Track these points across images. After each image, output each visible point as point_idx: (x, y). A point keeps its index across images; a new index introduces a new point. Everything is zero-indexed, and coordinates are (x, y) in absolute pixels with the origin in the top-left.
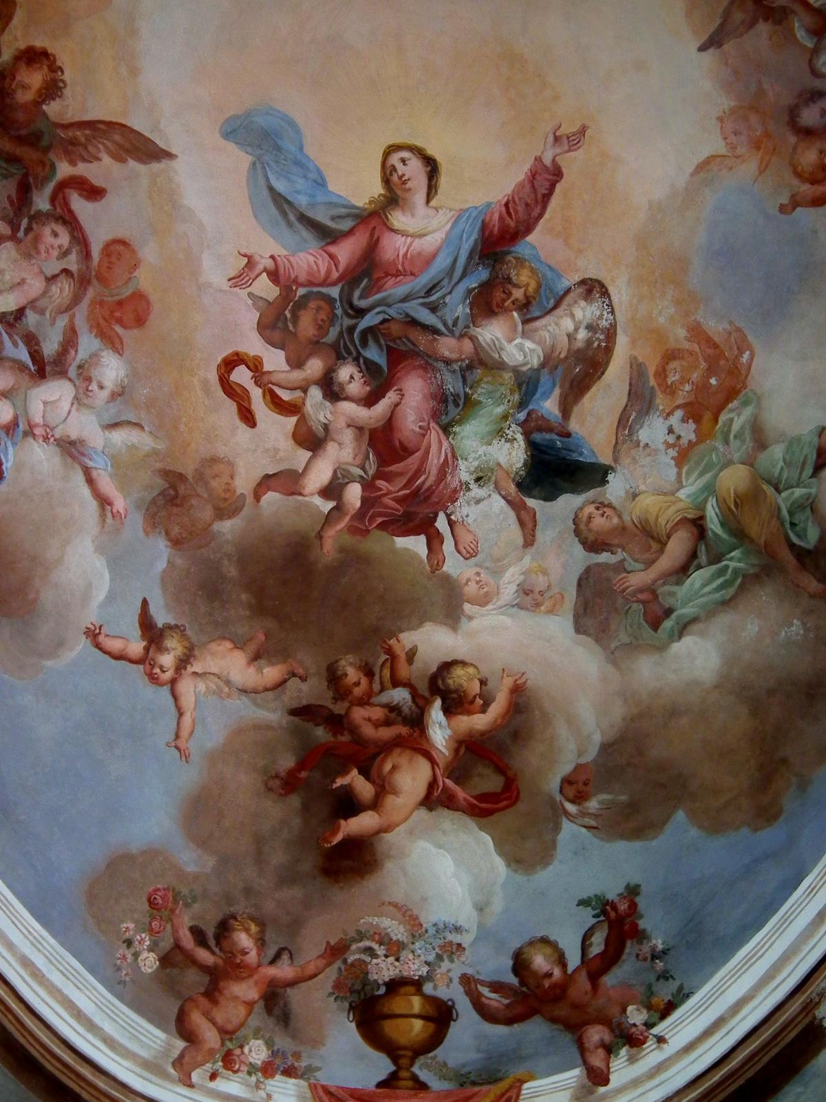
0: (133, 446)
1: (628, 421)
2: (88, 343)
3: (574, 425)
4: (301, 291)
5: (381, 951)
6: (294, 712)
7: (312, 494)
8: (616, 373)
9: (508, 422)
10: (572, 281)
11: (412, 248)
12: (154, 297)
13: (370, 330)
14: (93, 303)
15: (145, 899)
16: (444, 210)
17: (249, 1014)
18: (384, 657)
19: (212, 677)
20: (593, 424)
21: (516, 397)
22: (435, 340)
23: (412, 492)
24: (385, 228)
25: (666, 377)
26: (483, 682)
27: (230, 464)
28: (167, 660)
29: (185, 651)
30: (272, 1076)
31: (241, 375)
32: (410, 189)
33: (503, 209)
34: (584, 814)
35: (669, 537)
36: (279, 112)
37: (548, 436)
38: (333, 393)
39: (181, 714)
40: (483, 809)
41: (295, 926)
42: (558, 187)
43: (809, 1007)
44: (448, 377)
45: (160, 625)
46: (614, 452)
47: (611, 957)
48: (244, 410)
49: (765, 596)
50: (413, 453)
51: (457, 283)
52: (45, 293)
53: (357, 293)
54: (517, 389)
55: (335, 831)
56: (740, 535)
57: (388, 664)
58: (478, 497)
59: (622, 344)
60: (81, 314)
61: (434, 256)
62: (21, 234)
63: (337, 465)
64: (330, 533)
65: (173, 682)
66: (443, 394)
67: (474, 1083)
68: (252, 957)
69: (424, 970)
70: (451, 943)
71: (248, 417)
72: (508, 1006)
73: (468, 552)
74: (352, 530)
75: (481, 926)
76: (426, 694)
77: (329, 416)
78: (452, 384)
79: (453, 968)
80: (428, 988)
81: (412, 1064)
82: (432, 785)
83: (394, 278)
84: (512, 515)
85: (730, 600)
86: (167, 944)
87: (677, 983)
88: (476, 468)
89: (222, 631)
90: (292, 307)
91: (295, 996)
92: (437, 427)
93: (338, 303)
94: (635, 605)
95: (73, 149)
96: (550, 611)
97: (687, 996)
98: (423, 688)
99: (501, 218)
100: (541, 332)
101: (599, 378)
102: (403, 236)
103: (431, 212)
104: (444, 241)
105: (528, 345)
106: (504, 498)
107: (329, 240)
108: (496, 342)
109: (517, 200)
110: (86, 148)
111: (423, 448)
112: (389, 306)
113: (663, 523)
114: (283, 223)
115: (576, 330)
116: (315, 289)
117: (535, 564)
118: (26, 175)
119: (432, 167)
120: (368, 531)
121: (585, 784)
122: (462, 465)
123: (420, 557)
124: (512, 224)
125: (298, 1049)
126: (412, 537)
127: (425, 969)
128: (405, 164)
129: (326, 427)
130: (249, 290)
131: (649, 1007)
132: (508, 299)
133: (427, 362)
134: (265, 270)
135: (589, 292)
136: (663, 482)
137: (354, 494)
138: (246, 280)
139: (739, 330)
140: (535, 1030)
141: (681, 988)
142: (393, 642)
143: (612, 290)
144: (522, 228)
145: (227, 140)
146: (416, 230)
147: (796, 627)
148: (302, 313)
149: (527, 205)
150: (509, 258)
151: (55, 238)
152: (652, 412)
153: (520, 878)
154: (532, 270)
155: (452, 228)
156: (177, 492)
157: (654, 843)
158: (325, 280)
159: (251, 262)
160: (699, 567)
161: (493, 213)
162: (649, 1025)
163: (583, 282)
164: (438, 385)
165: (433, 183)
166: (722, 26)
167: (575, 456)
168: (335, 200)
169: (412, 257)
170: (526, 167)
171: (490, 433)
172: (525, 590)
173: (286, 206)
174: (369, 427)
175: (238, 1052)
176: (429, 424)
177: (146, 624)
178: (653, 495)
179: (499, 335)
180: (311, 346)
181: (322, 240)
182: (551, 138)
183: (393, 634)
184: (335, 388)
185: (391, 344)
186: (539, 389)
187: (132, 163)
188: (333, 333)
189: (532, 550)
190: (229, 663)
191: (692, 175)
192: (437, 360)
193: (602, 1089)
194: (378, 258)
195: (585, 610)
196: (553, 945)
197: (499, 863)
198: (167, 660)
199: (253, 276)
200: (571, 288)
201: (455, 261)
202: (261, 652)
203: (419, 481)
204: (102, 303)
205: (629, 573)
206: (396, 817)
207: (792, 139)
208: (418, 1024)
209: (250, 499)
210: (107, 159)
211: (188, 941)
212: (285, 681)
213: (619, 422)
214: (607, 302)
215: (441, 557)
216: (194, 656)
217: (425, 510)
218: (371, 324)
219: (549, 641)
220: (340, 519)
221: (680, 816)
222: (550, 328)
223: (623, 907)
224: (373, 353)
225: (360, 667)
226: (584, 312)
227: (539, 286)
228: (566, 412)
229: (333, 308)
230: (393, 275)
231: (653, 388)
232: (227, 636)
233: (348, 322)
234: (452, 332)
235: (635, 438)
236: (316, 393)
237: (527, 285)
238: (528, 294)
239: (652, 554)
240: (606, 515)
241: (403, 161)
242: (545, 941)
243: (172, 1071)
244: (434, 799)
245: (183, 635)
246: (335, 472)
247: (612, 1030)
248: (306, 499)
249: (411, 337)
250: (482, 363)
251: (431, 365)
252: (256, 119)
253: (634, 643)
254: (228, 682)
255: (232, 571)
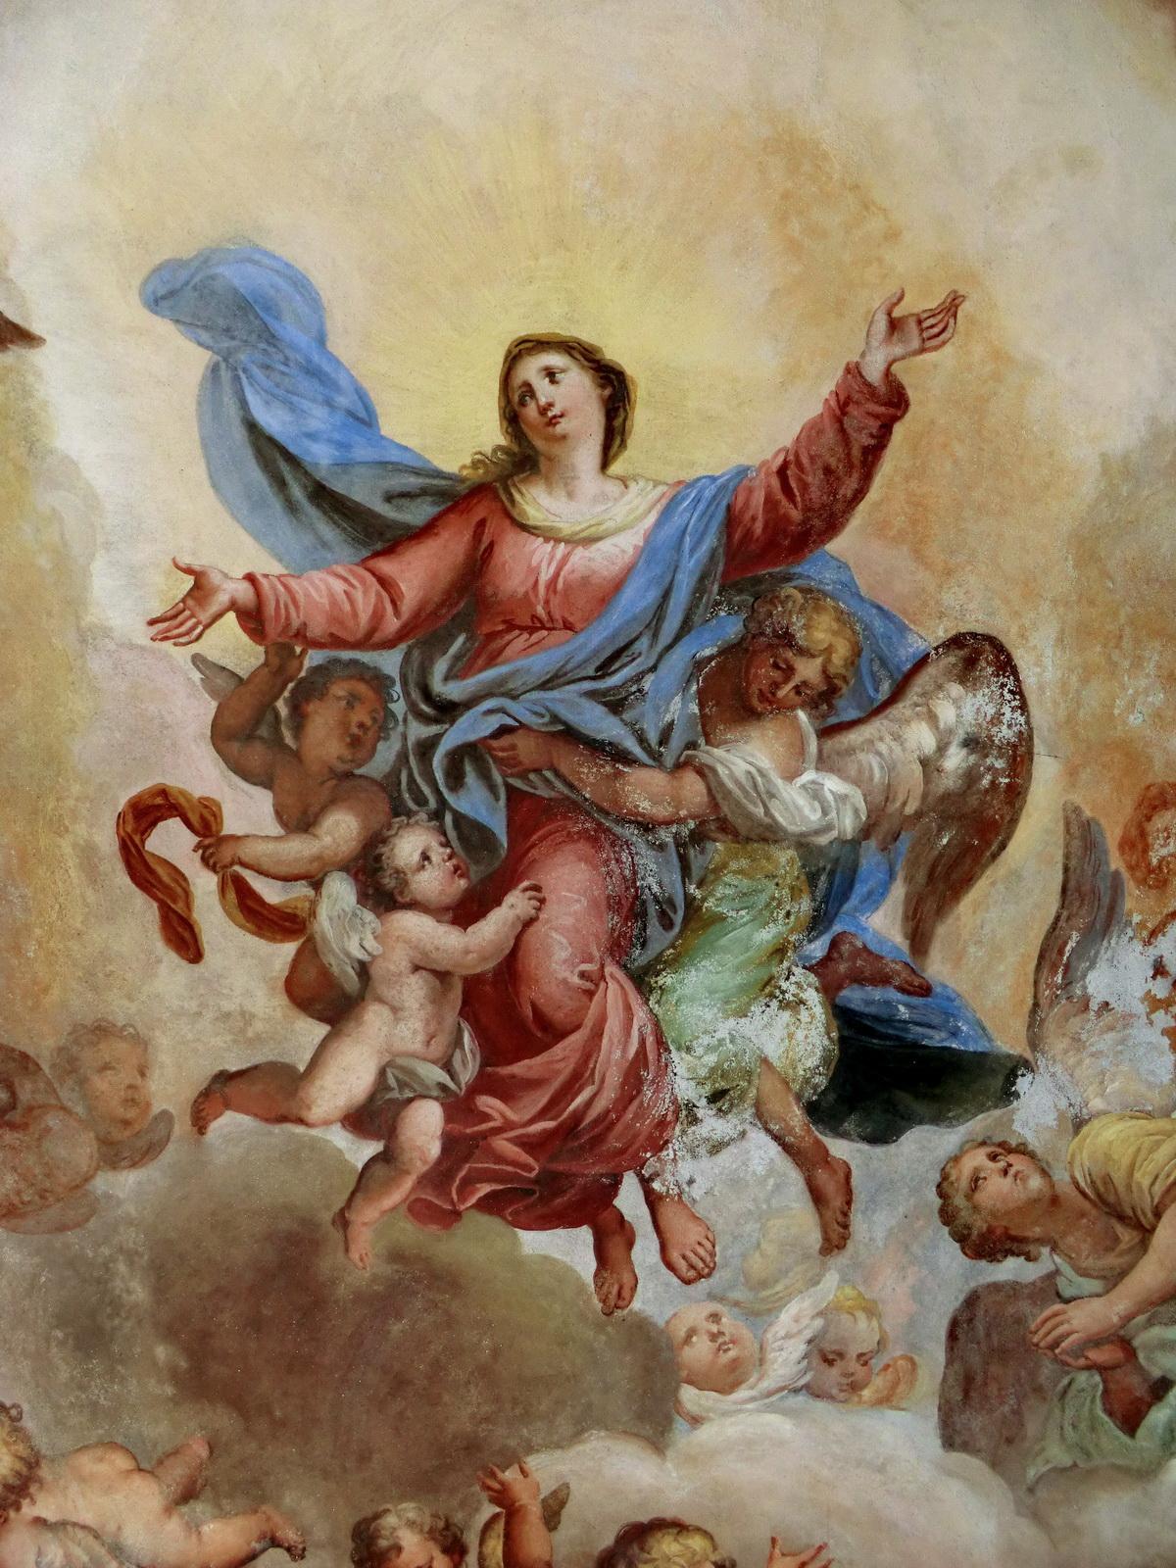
1: (1061, 953)
3: (937, 968)
4: (314, 658)
7: (327, 1123)
9: (786, 964)
10: (931, 639)
11: (567, 568)
13: (469, 752)
16: (642, 483)
18: (489, 1510)
19: (80, 1534)
20: (982, 960)
21: (805, 906)
22: (618, 774)
23: (560, 1126)
24: (507, 522)
25: (1146, 849)
27: (141, 1043)
29: (19, 1466)
31: (171, 841)
32: (564, 437)
33: (775, 483)
35: (1158, 1214)
36: (274, 257)
37: (877, 994)
38: (381, 892)
42: (899, 430)
44: (647, 860)
46: (1030, 1026)
48: (175, 921)
50: (563, 1035)
51: (670, 647)
53: (441, 666)
54: (805, 887)
57: (500, 1527)
58: (717, 1136)
59: (1046, 778)
61: (618, 585)
63: (387, 1058)
64: (368, 1215)
66: (636, 897)
71: (183, 938)
73: (692, 1267)
74: (418, 1210)
77: (371, 944)
78: (656, 874)
83: (526, 636)
84: (795, 1177)
88: (713, 1070)
90: (293, 692)
92: (620, 974)
93: (398, 688)
94: (1082, 1378)
96: (885, 1400)
99: (770, 502)
100: (861, 756)
101: (995, 856)
102: (547, 540)
103: (612, 488)
104: (640, 552)
105: (832, 784)
106: (777, 1138)
107: (379, 546)
108: (759, 779)
109: (805, 460)
111: (589, 1022)
112: (514, 697)
113: (1146, 1182)
114: (276, 505)
115: (942, 749)
116: (346, 655)
117: (849, 1291)
119: (614, 388)
120: (457, 1215)
122: (680, 1063)
123: (579, 1278)
124: (796, 515)
126: (560, 1232)
128: (553, 381)
129: (363, 970)
130: (195, 648)
132: (787, 680)
133: (599, 824)
134: (233, 605)
135: (970, 663)
136: (1143, 1089)
137: (425, 1127)
138: (190, 624)
142: (510, 1475)
143: (1022, 659)
144: (817, 522)
145: (156, 313)
146: (578, 528)
149: (828, 471)
150: (788, 590)
152: (1115, 930)
154: (841, 617)
155: (659, 524)
156: (13, 1094)
158: (373, 630)
159: (201, 587)
161: (750, 491)
163: (956, 642)
164: (624, 877)
165: (617, 423)
168: (394, 456)
169: (568, 587)
170: (827, 388)
171: (743, 989)
172: (825, 1354)
173: (285, 468)
174: (465, 972)
176: (602, 966)
178: (1121, 1118)
179: (765, 763)
180: (334, 782)
181: (365, 544)
182: (882, 324)
184: (386, 881)
185: (517, 783)
186: (857, 886)
189: (841, 1259)
192: (621, 821)
194: (489, 590)
195: (966, 1393)
199: (204, 617)
200: (928, 655)
201: (666, 595)
202: (198, 1486)
203: (579, 1101)
205: (1067, 1301)
209: (182, 1126)
213: (1041, 957)
214: (1011, 683)
215: (626, 1278)
216: (40, 1482)
217: (594, 1170)
218: (472, 737)
219: (881, 1469)
220: (389, 1184)
222: (883, 748)
224: (476, 801)
225: (431, 1531)
226: (959, 708)
227: (857, 652)
228: (919, 938)
230: (523, 629)
231: (1116, 874)
232: (119, 1440)
233: (418, 731)
234: (657, 757)
235: (1079, 992)
236: (341, 891)
237: (829, 650)
238: (832, 670)
239: (1121, 1255)
240: (1012, 1171)
241: (551, 374)
246: (382, 1073)
248: (314, 1132)
249: (564, 769)
250: (725, 827)
251: (608, 830)
252: (220, 270)
253: (1081, 1464)
255: (137, 1291)
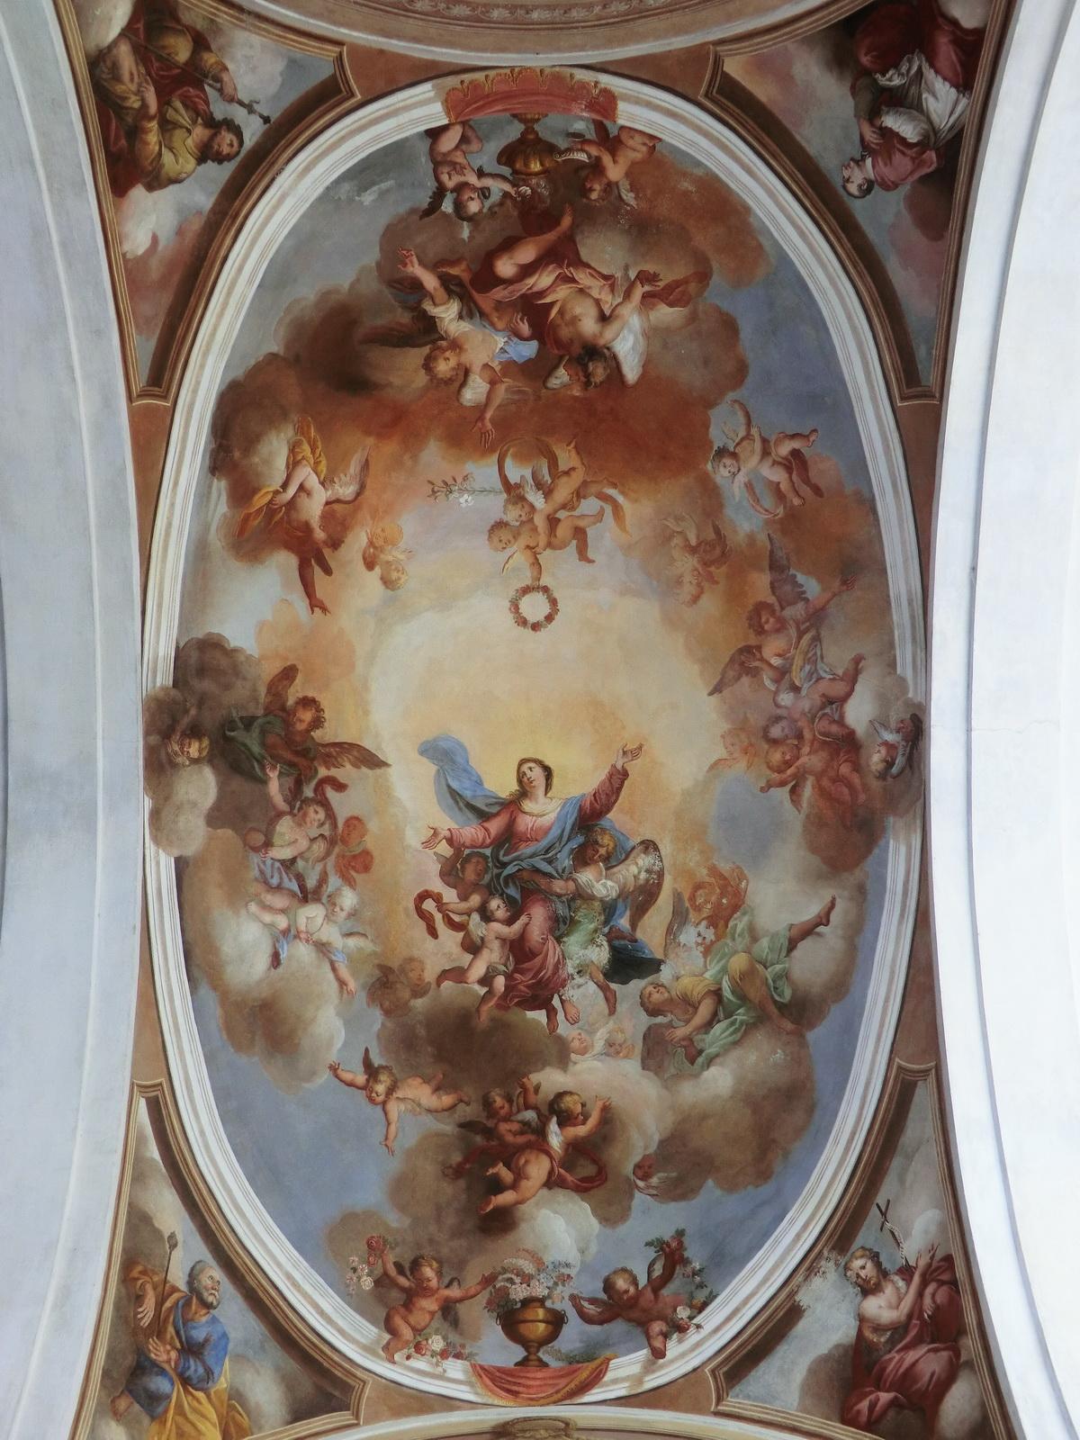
0: (362, 948)
2: (334, 881)
3: (639, 935)
4: (467, 851)
5: (518, 1280)
6: (462, 1126)
8: (664, 901)
12: (376, 854)
14: (338, 856)
15: (365, 1242)
17: (432, 1319)
18: (519, 1090)
20: (651, 932)
21: (603, 918)
26: (583, 1105)
27: (421, 962)
28: (381, 1088)
30: (447, 1358)
31: (429, 905)
34: (648, 1187)
37: (622, 942)
38: (487, 917)
39: (389, 1124)
40: (583, 1188)
41: (461, 1265)
43: (792, 1294)
44: (559, 906)
45: (376, 1065)
47: (667, 1277)
49: (760, 1036)
52: (309, 848)
53: (502, 853)
55: (488, 1203)
56: (743, 998)
60: (331, 861)
61: (550, 829)
62: (296, 811)
64: (485, 1008)
65: (384, 1103)
67: (578, 1362)
68: (434, 1283)
69: (546, 1292)
70: (563, 1274)
71: (433, 932)
72: (600, 1313)
74: (498, 1006)
75: (582, 1262)
76: (547, 1113)
78: (562, 910)
79: (564, 1292)
80: (548, 1304)
81: (538, 1351)
82: (551, 1173)
84: (601, 994)
85: (739, 1041)
86: (379, 1271)
87: (709, 1289)
89: (415, 1071)
91: (462, 1309)
95: (329, 760)
96: (626, 1057)
97: (715, 1297)
98: (545, 1110)
103: (548, 800)
105: (609, 883)
110: (336, 759)
114: (456, 809)
115: (639, 873)
118: (300, 775)
119: (548, 772)
121: (650, 1167)
122: (569, 962)
124: (598, 807)
125: (463, 1342)
127: (546, 1292)
131: (691, 1307)
134: (445, 838)
135: (647, 848)
137: (500, 982)
139: (738, 867)
140: (618, 1327)
141: (711, 1292)
142: (525, 1080)
147: (779, 1055)
148: (467, 866)
150: (597, 828)
151: (316, 815)
153: (608, 1231)
157: (694, 1202)
159: (436, 833)
160: (719, 1021)
162: (691, 1318)
163: (642, 842)
166: (721, 679)
167: (640, 954)
168: (488, 794)
170: (606, 771)
175: (425, 1342)
177: (367, 1064)
183: (525, 1075)
187: (364, 769)
188: (487, 878)
189: (614, 1017)
190: (419, 1092)
191: (708, 772)
193: (661, 1361)
196: (630, 1273)
197: (594, 1222)
198: (381, 1088)
201: (563, 832)
204: (343, 856)
206: (528, 1195)
207: (766, 747)
208: (542, 1326)
209: (434, 986)
210: (348, 766)
211: (392, 1271)
212: (456, 1105)
220: (490, 1000)
221: (710, 1183)
223: (674, 1245)
228: (634, 925)
229: (487, 862)
233: (496, 871)
234: (562, 877)
236: (476, 917)
241: (530, 769)
242: (624, 1270)
243: (382, 1353)
244: (552, 1182)
245: (391, 1073)
247: (668, 1324)
250: (580, 896)
254: (419, 1105)
255: (422, 1032)
